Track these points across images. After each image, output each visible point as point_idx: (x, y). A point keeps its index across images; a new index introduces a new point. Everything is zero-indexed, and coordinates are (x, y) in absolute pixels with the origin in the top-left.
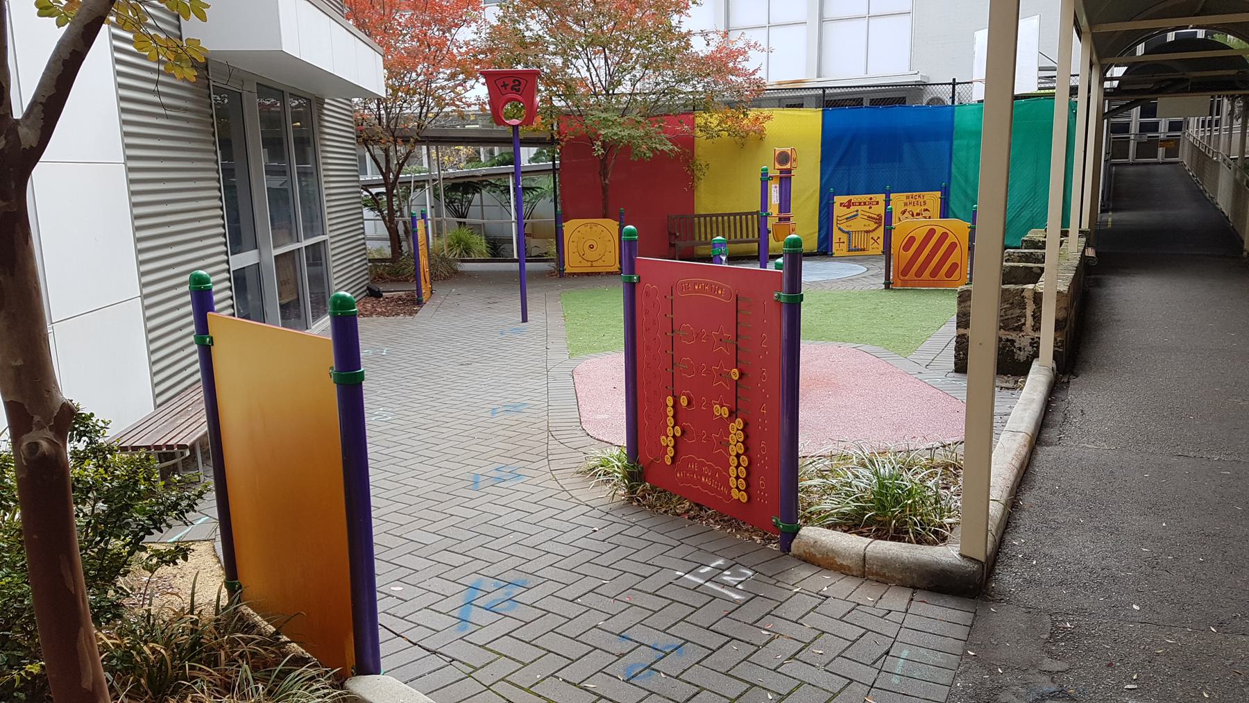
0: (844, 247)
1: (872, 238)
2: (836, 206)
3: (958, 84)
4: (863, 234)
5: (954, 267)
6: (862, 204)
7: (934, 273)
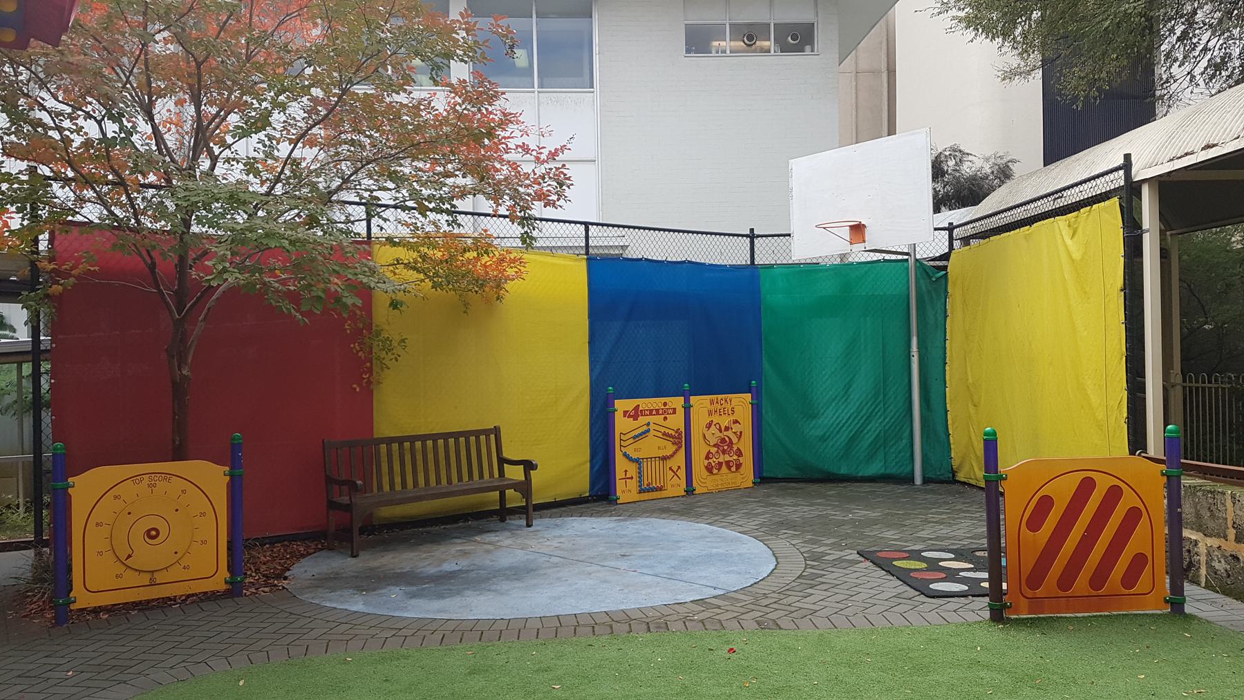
0: (633, 485)
1: (670, 468)
2: (619, 416)
3: (759, 236)
4: (657, 462)
5: (1139, 562)
6: (654, 412)
7: (1098, 579)
